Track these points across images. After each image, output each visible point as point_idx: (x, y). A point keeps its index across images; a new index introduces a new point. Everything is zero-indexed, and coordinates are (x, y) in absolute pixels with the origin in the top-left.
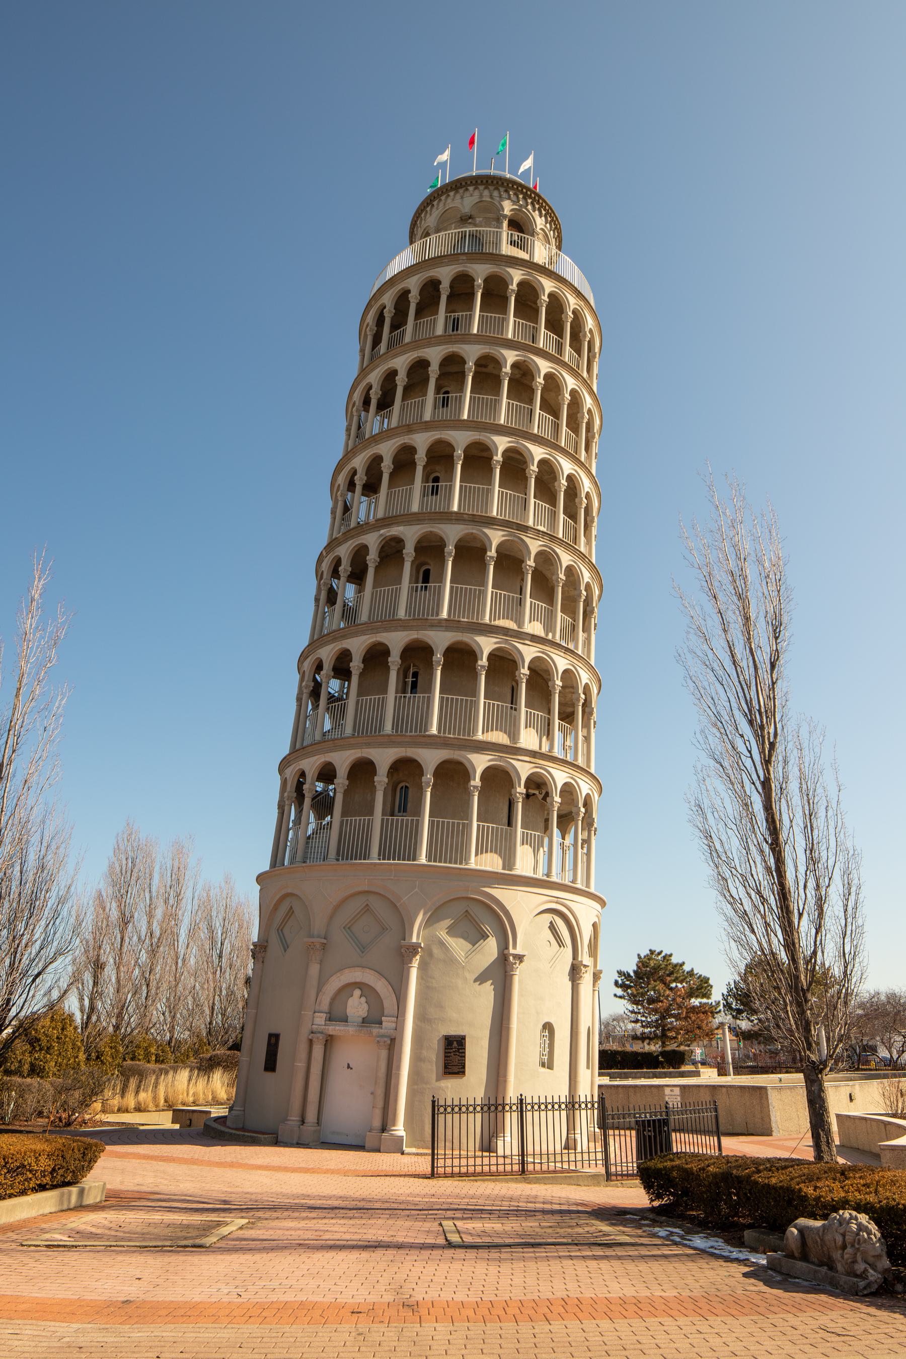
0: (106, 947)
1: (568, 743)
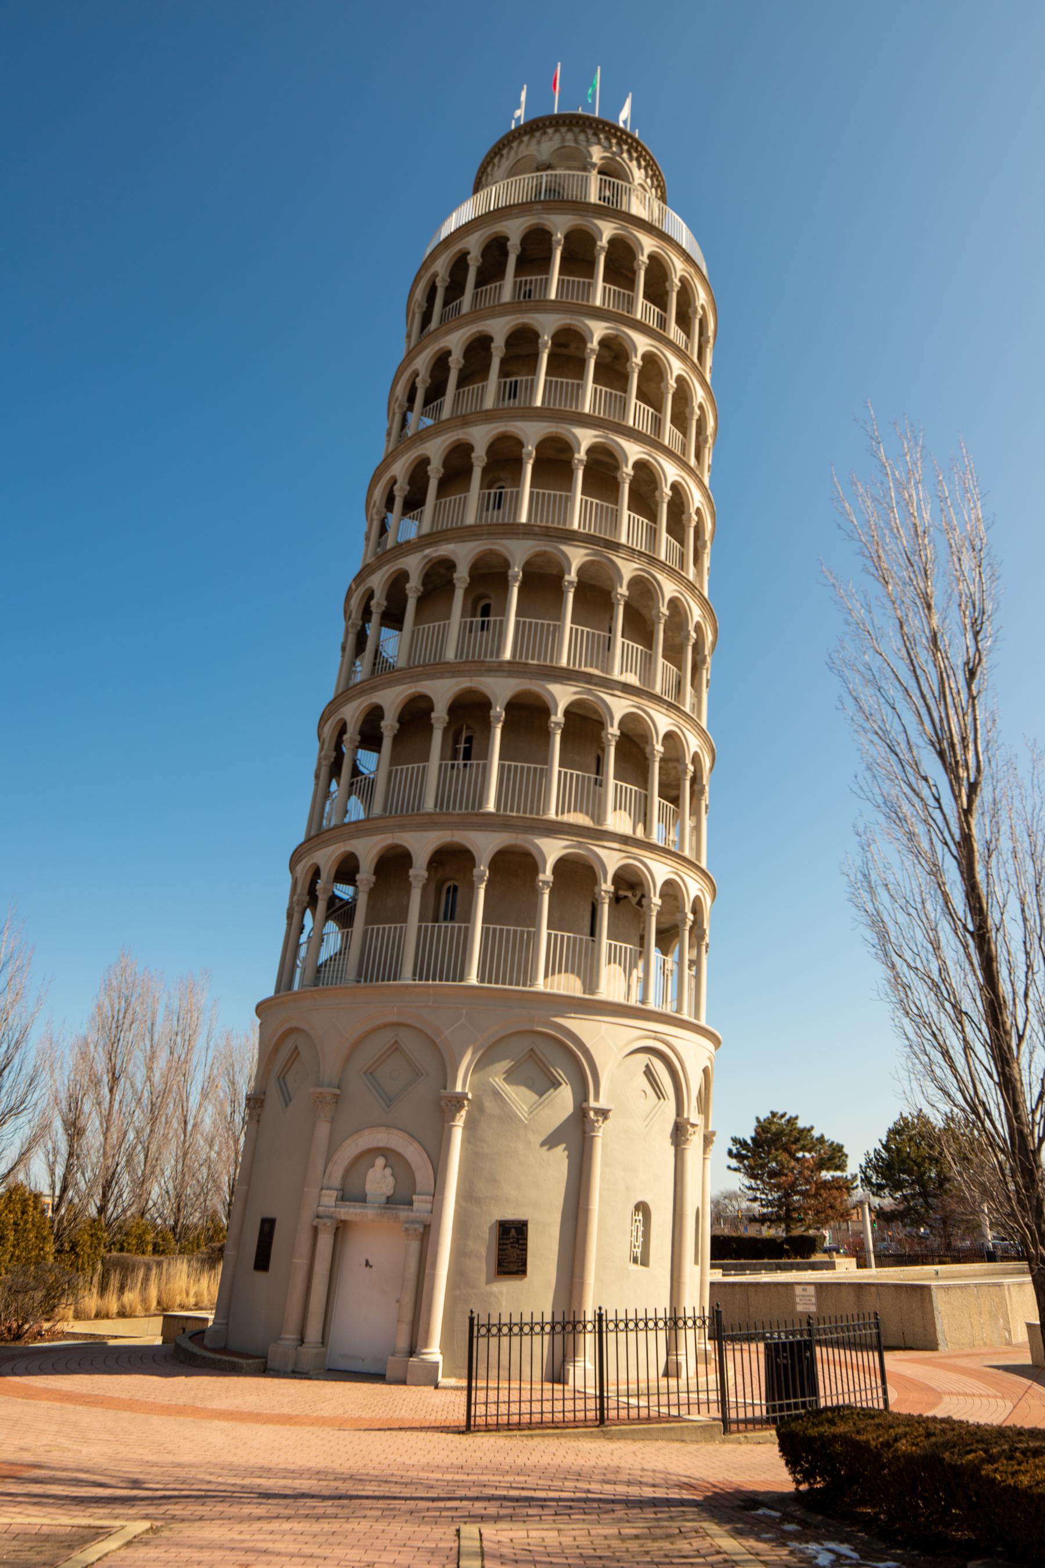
0: (87, 1106)
1: (671, 837)
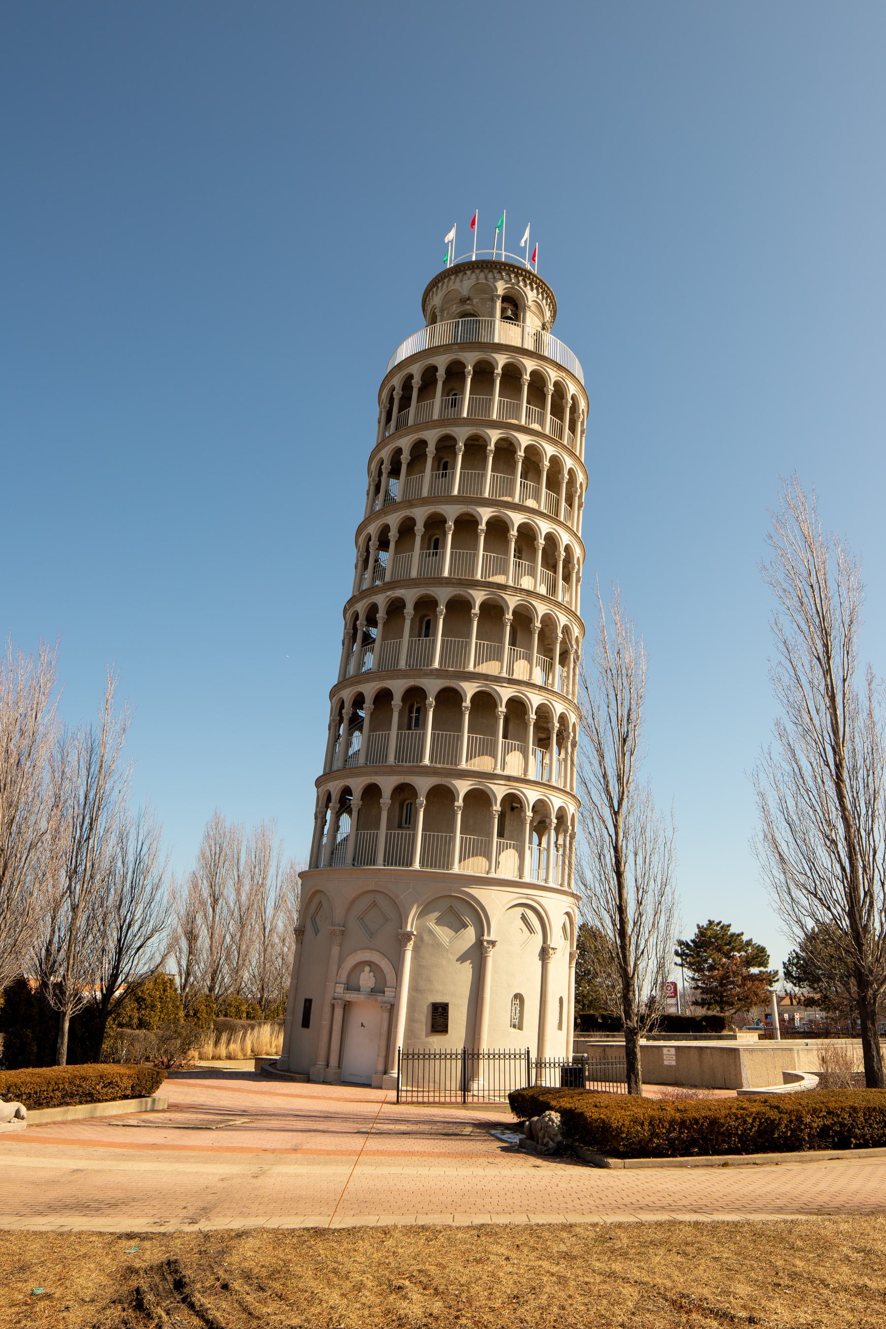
0: (199, 920)
